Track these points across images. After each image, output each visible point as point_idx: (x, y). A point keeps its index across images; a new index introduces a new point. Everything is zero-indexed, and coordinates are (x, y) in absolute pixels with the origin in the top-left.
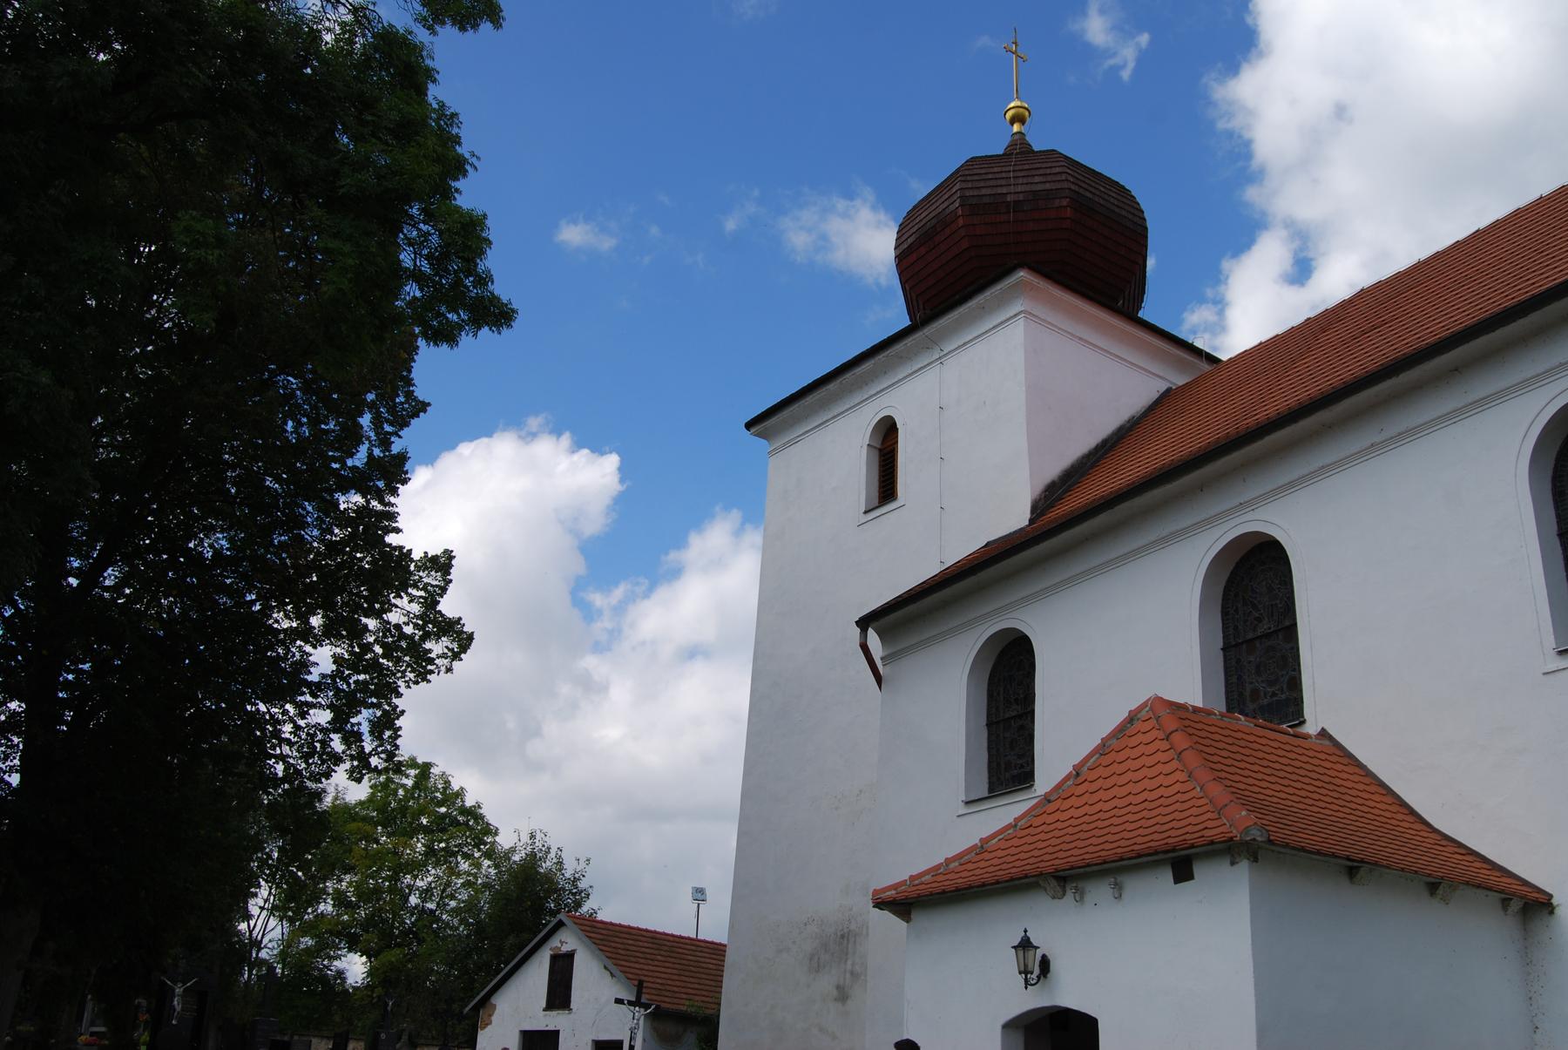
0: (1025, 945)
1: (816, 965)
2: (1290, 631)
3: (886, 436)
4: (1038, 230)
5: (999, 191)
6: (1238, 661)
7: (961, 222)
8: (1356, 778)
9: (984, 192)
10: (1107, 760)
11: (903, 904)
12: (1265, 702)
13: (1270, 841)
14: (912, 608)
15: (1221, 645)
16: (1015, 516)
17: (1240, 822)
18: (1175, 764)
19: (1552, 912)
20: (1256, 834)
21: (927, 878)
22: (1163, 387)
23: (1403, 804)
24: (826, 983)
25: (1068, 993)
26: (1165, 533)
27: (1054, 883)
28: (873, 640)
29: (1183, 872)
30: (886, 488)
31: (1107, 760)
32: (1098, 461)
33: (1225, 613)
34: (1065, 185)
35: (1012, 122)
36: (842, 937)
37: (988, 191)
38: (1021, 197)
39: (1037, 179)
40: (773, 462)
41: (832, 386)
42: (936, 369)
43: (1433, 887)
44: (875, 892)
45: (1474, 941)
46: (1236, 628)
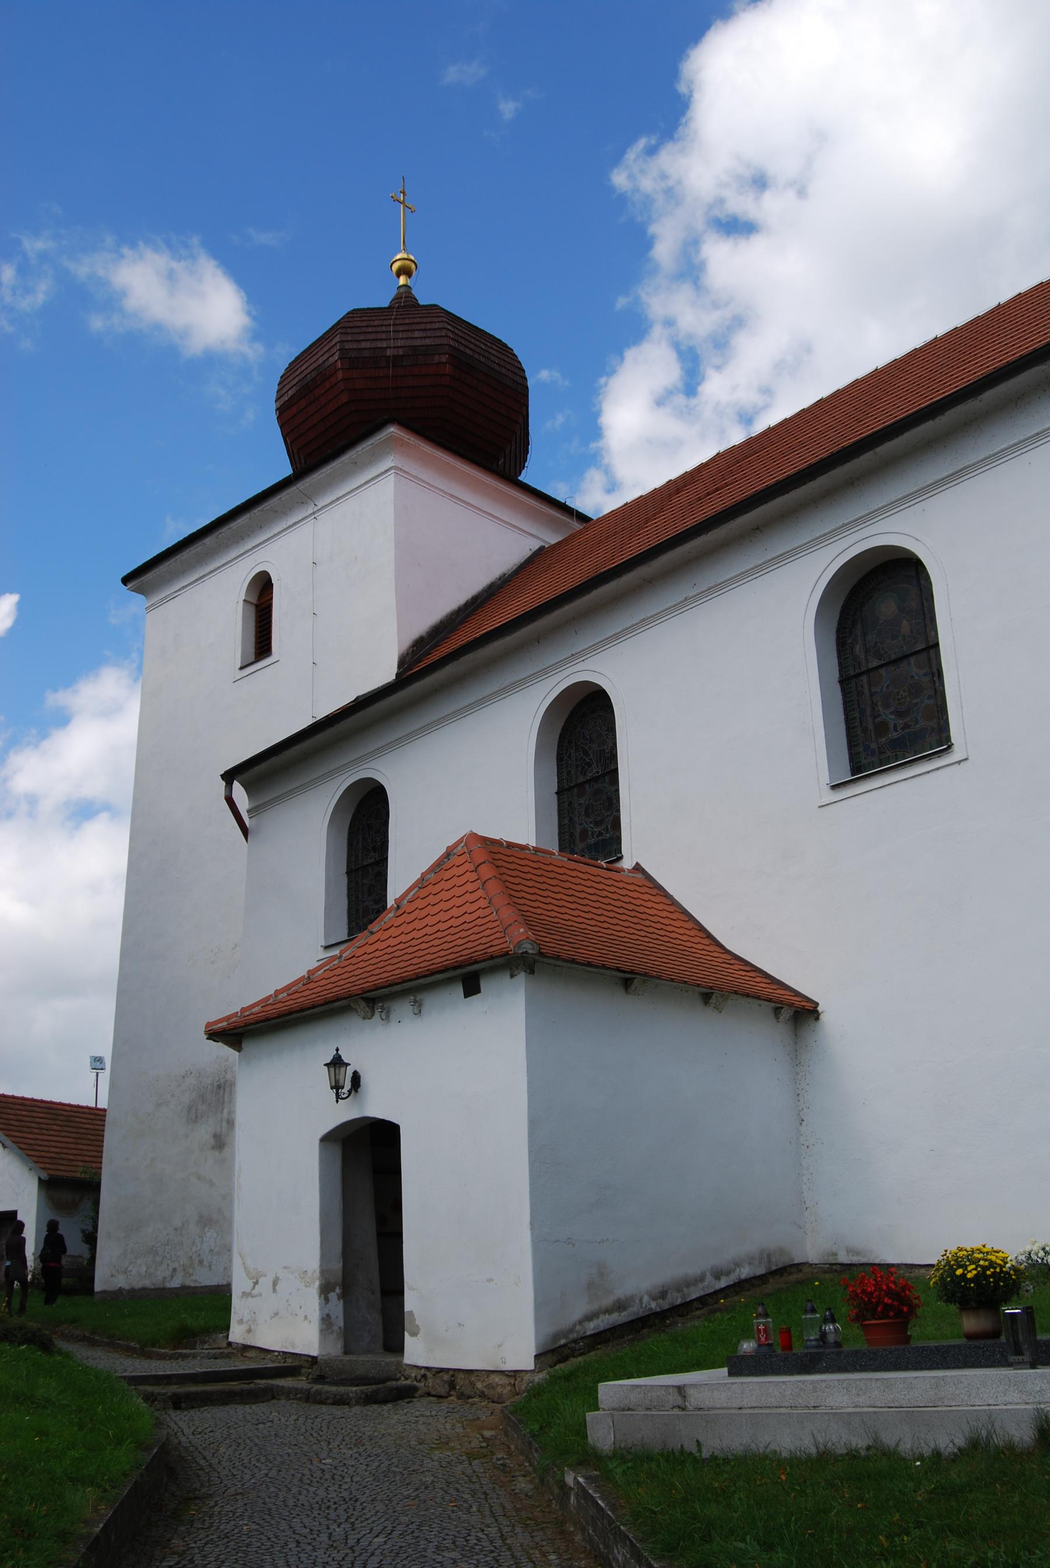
0: (337, 1063)
1: (193, 1116)
2: (612, 775)
3: (262, 589)
4: (411, 386)
5: (379, 344)
6: (570, 804)
7: (340, 375)
8: (661, 907)
9: (364, 345)
10: (424, 893)
11: (235, 1034)
12: (592, 841)
13: (541, 954)
14: (274, 760)
15: (555, 789)
16: (387, 673)
17: (519, 937)
18: (480, 893)
19: (817, 1018)
20: (528, 947)
21: (257, 1009)
22: (535, 545)
23: (702, 929)
24: (204, 1132)
25: (375, 1105)
26: (506, 683)
27: (363, 1004)
28: (239, 791)
29: (472, 988)
30: (261, 644)
31: (424, 893)
32: (468, 616)
33: (560, 759)
34: (445, 341)
35: (398, 275)
36: (219, 1087)
37: (368, 345)
38: (401, 352)
39: (417, 334)
40: (150, 617)
41: (209, 541)
42: (310, 522)
43: (706, 998)
44: (208, 1024)
45: (747, 1044)
46: (569, 773)
